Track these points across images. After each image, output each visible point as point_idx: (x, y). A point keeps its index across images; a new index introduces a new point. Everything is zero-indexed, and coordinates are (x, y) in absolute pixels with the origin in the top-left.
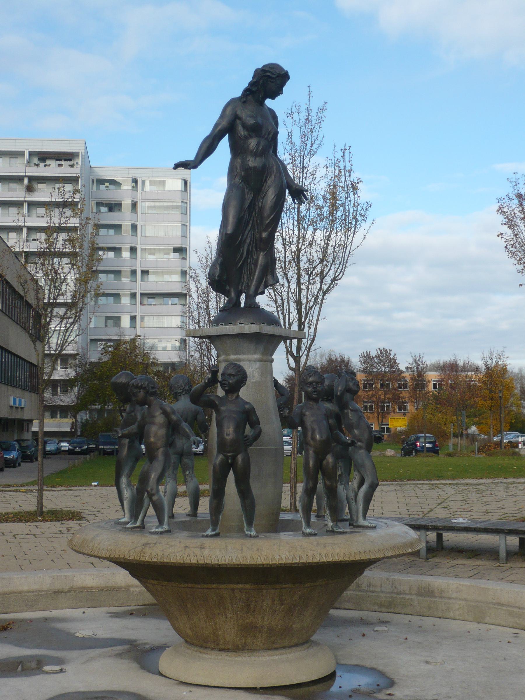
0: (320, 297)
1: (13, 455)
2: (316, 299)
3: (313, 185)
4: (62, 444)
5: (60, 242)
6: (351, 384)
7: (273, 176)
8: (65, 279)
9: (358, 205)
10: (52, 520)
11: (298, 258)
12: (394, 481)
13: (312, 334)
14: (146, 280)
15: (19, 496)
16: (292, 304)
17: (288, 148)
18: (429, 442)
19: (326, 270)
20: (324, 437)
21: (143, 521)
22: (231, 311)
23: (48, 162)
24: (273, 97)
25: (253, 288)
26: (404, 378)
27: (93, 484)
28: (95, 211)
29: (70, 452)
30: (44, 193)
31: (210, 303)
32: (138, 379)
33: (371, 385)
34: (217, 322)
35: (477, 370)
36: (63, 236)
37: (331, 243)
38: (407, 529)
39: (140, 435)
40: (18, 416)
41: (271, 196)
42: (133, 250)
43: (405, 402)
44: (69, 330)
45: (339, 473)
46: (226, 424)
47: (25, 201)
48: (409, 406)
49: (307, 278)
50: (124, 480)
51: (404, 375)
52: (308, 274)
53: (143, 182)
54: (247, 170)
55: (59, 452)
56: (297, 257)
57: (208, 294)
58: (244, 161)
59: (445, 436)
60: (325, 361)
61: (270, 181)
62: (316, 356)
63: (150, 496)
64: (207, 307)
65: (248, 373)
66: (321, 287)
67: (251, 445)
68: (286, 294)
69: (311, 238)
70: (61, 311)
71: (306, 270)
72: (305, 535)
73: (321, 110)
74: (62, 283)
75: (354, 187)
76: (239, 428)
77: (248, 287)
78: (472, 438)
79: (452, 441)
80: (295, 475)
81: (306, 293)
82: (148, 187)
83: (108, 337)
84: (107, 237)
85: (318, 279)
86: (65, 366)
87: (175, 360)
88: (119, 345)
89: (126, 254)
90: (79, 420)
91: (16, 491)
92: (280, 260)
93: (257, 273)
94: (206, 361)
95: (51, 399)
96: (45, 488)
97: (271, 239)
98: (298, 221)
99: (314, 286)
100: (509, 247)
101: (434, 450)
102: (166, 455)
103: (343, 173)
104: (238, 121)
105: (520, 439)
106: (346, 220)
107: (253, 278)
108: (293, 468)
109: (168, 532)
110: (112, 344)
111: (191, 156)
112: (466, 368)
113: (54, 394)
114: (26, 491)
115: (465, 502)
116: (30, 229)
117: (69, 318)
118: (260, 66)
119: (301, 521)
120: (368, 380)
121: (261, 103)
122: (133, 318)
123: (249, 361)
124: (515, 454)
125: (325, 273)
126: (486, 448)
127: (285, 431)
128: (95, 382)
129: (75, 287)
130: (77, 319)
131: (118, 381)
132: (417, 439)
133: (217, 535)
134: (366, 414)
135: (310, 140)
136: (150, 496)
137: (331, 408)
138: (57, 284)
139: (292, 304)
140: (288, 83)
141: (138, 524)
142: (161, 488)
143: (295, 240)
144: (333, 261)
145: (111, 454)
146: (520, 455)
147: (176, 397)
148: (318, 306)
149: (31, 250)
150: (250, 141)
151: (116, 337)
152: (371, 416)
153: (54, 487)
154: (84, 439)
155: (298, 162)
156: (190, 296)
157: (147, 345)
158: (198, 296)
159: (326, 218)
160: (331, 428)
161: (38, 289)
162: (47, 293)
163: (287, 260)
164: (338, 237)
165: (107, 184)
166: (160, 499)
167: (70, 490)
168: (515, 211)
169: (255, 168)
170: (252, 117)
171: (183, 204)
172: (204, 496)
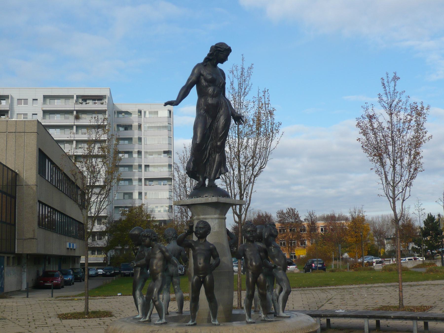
0: (253, 179)
1: (69, 278)
2: (250, 180)
3: (246, 113)
4: (99, 271)
5: (96, 149)
6: (273, 231)
7: (223, 109)
8: (99, 171)
9: (274, 124)
10: (94, 317)
11: (239, 156)
12: (300, 288)
13: (248, 201)
14: (147, 170)
15: (74, 303)
16: (235, 183)
17: (231, 91)
18: (320, 264)
19: (256, 162)
20: (258, 264)
21: (150, 317)
22: (199, 190)
23: (88, 101)
24: (222, 63)
25: (213, 175)
26: (304, 225)
27: (118, 294)
28: (116, 130)
29: (103, 275)
30: (86, 120)
31: (186, 184)
32: (145, 232)
33: (284, 230)
34: (192, 196)
35: (347, 219)
36: (97, 146)
37: (258, 147)
38: (309, 317)
39: (148, 265)
40: (72, 254)
41: (222, 120)
42: (139, 153)
43: (305, 240)
44: (103, 202)
45: (267, 285)
46: (199, 257)
47: (74, 125)
48: (307, 242)
49: (244, 168)
50: (138, 293)
51: (303, 223)
52: (245, 165)
53: (145, 112)
54: (208, 105)
55: (97, 275)
56: (238, 156)
57: (185, 179)
58: (206, 101)
59: (330, 259)
60: (256, 216)
61: (221, 112)
62: (250, 214)
63: (154, 302)
64: (185, 186)
65: (211, 226)
66: (253, 173)
67: (214, 269)
68: (232, 178)
69: (246, 144)
70: (97, 190)
71: (244, 163)
72: (248, 323)
73: (250, 68)
74: (98, 174)
75: (271, 113)
76: (207, 260)
77: (210, 175)
78: (345, 261)
79: (334, 262)
80: (241, 286)
81: (244, 177)
82: (147, 115)
83: (125, 205)
84: (124, 145)
85: (251, 168)
86: (99, 223)
87: (166, 218)
88: (132, 210)
89: (135, 155)
90: (109, 256)
91: (71, 300)
92: (228, 157)
93: (215, 166)
94: (185, 219)
95: (91, 243)
96: (89, 298)
97: (223, 146)
98: (238, 134)
99: (249, 172)
100: (364, 146)
101: (323, 269)
102: (163, 277)
103: (264, 105)
104: (202, 77)
105: (374, 260)
106: (266, 133)
107: (213, 170)
108: (239, 282)
109: (165, 323)
110: (127, 209)
111: (174, 98)
112: (339, 218)
113: (94, 240)
114: (78, 299)
115: (343, 299)
116: (78, 142)
117: (102, 195)
118: (214, 44)
119: (245, 315)
120: (282, 227)
121: (215, 66)
122: (140, 194)
123: (212, 219)
124: (371, 269)
125: (255, 164)
126: (355, 266)
127: (233, 260)
128: (118, 232)
129: (105, 176)
130: (107, 195)
131: (133, 233)
132: (313, 262)
133: (195, 325)
134: (282, 248)
135: (244, 86)
136: (154, 302)
137: (261, 246)
138: (95, 175)
139: (235, 183)
140: (231, 54)
141: (147, 319)
142: (161, 296)
143: (237, 145)
144: (260, 157)
145: (128, 276)
146: (374, 270)
147: (168, 241)
148: (251, 184)
149: (79, 154)
150: (209, 88)
151: (130, 205)
152: (284, 249)
153: (94, 297)
154: (112, 267)
155: (237, 99)
156: (174, 180)
157: (149, 210)
158: (180, 179)
159: (255, 132)
160: (262, 258)
161: (84, 178)
162: (89, 179)
163: (232, 157)
164: (262, 143)
165: (123, 114)
166: (160, 304)
167: (104, 299)
168: (368, 125)
169: (212, 105)
170: (210, 74)
171: (169, 125)
172: (185, 300)
